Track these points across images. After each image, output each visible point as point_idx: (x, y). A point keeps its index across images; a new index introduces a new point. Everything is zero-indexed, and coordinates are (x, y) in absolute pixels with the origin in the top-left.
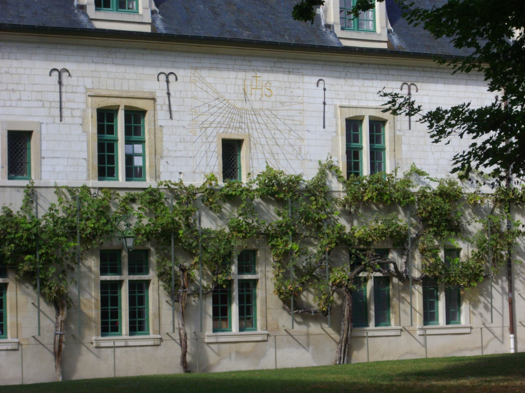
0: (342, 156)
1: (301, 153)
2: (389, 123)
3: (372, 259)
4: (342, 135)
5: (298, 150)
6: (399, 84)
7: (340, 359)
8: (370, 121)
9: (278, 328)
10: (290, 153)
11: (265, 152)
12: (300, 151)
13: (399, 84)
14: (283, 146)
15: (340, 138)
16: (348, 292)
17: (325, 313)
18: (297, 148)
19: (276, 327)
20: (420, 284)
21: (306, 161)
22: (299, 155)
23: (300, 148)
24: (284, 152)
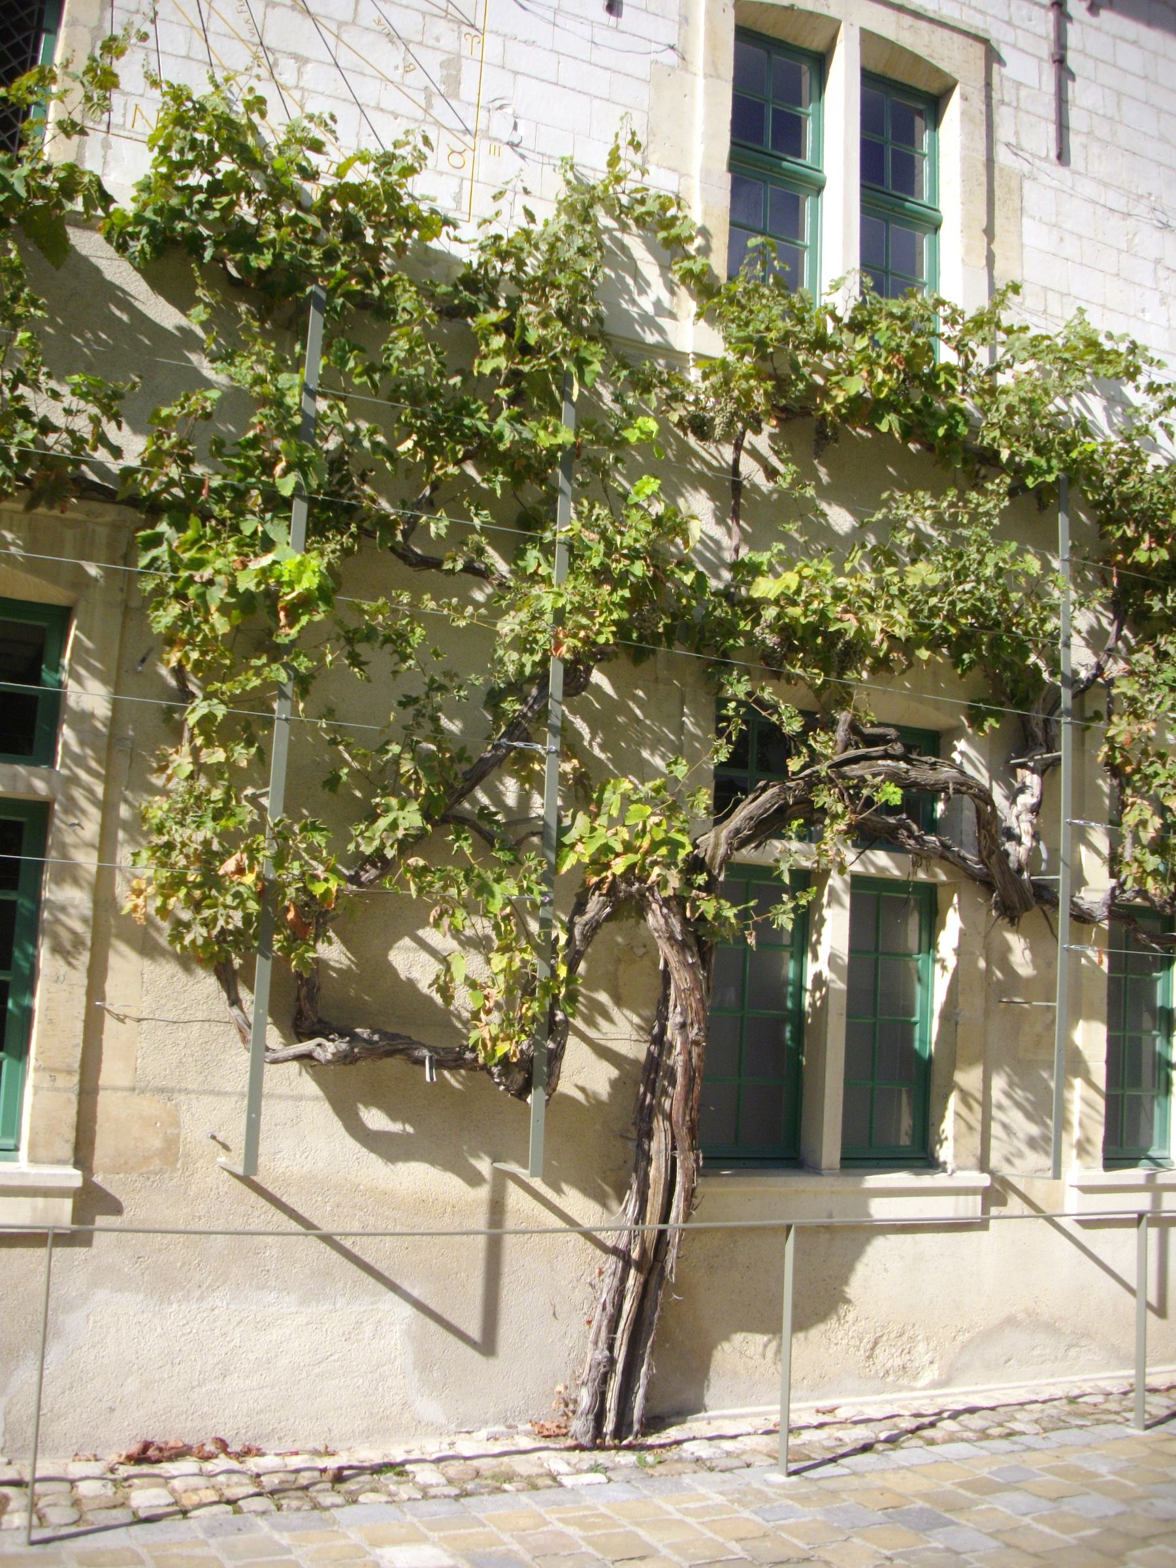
0: (706, 173)
1: (456, 96)
2: (965, 98)
3: (852, 752)
4: (712, 74)
5: (437, 74)
6: (677, 885)
7: (605, 1379)
8: (870, 79)
9: (171, 1151)
10: (385, 79)
11: (214, 25)
12: (453, 81)
13: (677, 885)
14: (341, 24)
15: (700, 82)
16: (683, 947)
17: (519, 1078)
18: (431, 61)
19: (157, 1143)
20: (71, 709)
21: (483, 146)
22: (437, 101)
23: (453, 64)
24: (346, 58)
